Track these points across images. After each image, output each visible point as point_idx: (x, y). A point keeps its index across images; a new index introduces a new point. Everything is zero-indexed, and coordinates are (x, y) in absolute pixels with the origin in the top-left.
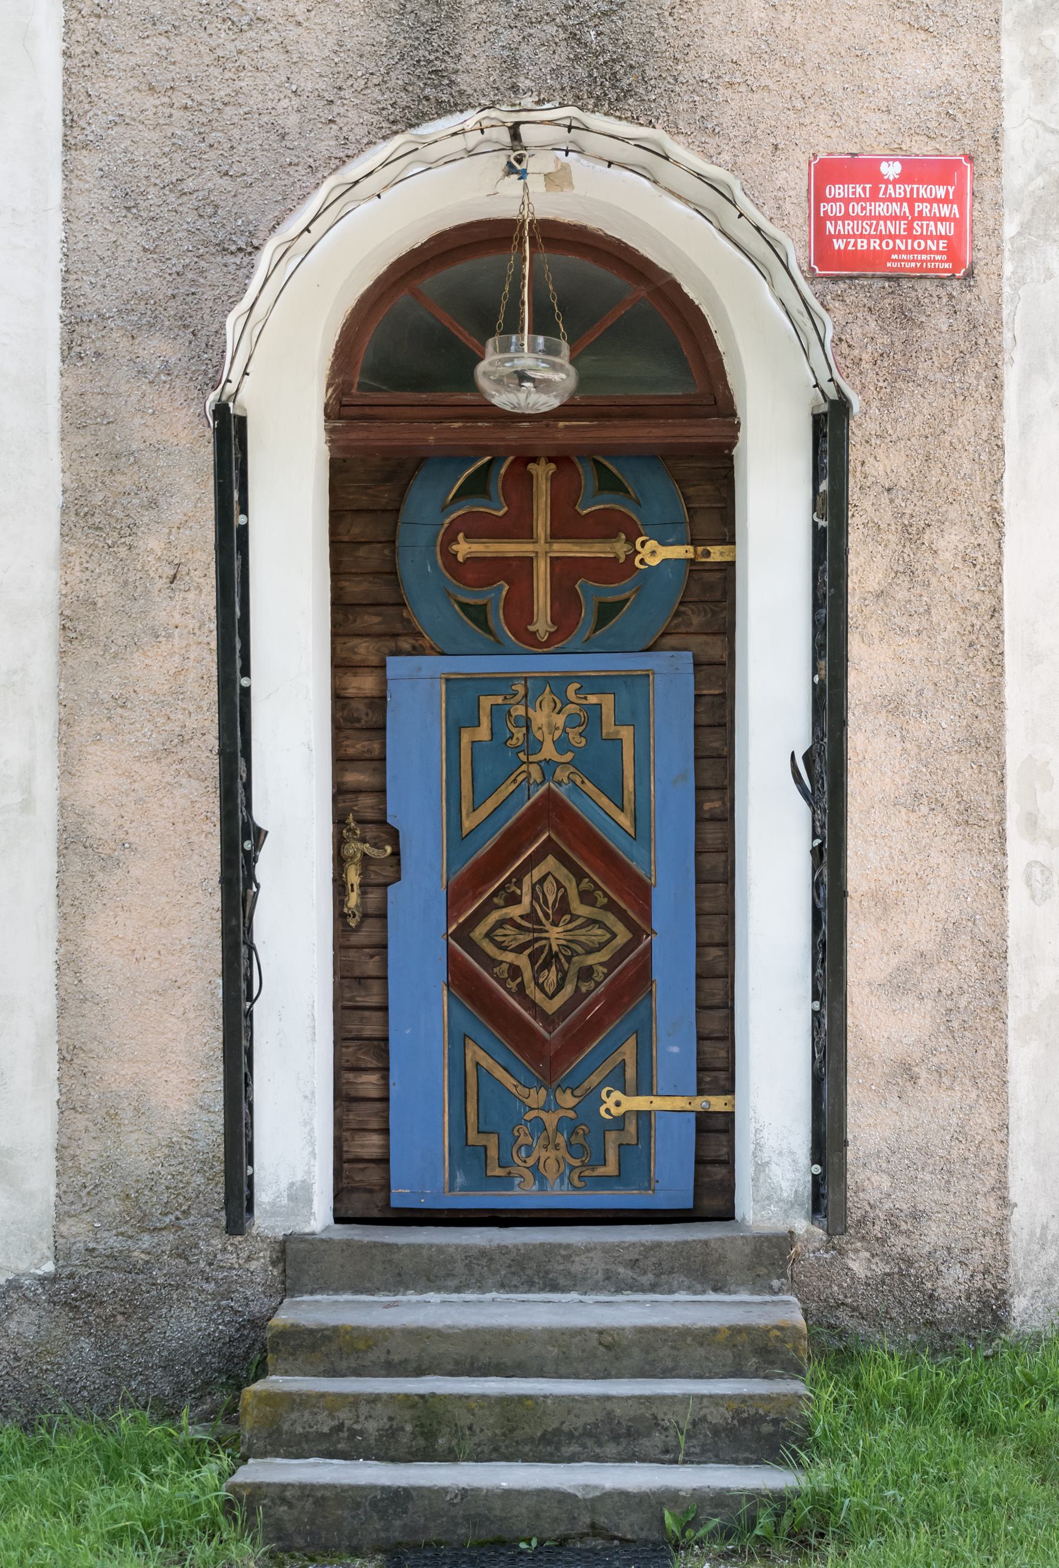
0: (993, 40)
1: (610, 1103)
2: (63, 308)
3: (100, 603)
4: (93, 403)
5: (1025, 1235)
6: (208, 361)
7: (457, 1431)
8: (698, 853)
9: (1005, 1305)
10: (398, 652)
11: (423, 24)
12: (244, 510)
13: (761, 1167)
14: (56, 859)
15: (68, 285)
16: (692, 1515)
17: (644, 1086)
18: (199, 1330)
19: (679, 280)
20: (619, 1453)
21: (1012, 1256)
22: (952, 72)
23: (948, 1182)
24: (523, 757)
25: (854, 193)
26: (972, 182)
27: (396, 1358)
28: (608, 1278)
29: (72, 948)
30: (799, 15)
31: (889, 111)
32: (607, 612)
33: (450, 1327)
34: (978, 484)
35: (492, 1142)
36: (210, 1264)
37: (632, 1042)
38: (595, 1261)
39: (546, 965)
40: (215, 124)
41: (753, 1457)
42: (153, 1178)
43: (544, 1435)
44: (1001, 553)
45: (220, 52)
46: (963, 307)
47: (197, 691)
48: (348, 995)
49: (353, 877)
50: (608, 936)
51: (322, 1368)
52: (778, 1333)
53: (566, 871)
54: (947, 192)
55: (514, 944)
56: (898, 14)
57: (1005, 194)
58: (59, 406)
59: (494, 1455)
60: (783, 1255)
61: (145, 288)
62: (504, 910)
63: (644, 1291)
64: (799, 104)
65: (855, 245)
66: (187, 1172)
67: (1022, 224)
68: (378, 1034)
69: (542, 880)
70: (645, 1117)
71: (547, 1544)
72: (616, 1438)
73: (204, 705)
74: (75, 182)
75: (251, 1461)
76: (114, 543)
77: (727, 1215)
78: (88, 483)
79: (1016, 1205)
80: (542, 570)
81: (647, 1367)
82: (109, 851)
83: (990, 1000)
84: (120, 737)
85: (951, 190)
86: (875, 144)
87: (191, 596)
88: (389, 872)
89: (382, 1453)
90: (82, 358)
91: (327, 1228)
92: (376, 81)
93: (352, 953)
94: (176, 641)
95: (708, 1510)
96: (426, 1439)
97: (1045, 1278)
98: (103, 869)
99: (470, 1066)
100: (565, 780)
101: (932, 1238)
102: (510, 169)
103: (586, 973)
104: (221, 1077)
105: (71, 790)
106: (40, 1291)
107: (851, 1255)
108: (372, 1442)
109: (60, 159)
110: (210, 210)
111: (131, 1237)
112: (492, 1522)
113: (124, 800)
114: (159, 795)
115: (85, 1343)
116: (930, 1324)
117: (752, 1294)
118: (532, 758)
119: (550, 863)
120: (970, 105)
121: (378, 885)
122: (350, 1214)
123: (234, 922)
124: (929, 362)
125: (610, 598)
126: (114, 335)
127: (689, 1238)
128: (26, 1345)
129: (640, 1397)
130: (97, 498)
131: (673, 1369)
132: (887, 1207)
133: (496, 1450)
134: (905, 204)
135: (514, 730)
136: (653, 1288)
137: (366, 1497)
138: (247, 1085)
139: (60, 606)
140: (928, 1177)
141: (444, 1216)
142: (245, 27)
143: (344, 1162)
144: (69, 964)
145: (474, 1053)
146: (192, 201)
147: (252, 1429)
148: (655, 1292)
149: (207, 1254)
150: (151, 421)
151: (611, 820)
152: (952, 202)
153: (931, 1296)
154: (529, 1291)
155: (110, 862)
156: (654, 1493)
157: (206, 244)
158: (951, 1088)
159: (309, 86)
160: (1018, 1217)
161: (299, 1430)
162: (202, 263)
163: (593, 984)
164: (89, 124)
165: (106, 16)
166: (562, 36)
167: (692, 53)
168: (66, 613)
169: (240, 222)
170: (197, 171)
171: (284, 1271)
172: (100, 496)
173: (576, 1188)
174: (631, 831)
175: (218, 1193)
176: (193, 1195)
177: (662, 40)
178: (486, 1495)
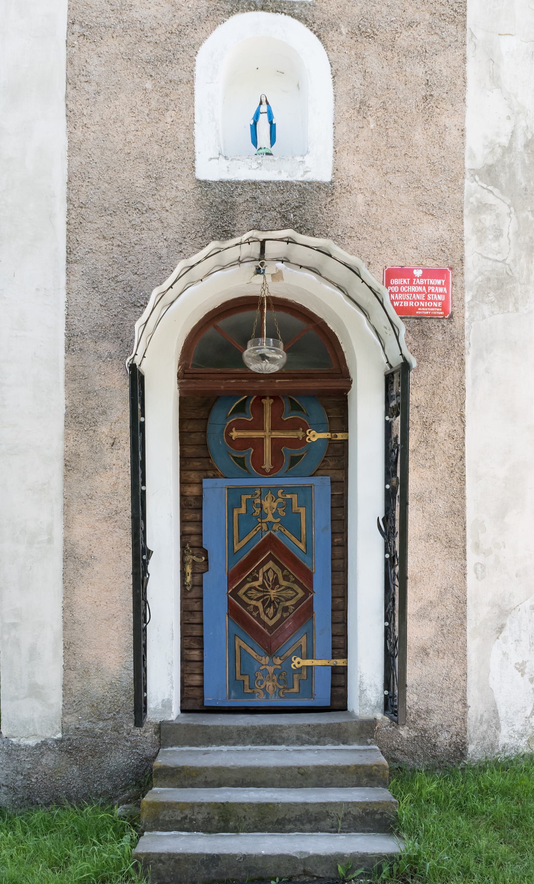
0: (460, 220)
1: (295, 663)
2: (66, 330)
3: (81, 454)
4: (79, 370)
5: (473, 719)
6: (126, 344)
7: (238, 819)
8: (332, 559)
9: (465, 748)
10: (207, 477)
11: (220, 211)
12: (143, 415)
13: (362, 692)
14: (62, 563)
15: (68, 320)
16: (350, 866)
17: (310, 655)
18: (124, 762)
19: (326, 322)
20: (311, 828)
21: (468, 728)
22: (443, 233)
23: (442, 697)
24: (259, 520)
25: (402, 282)
26: (452, 278)
27: (209, 780)
28: (298, 739)
29: (69, 601)
30: (379, 208)
31: (417, 249)
32: (294, 460)
33: (233, 766)
34: (455, 404)
35: (246, 679)
36: (128, 734)
37: (305, 637)
38: (293, 732)
39: (269, 606)
40: (131, 253)
41: (372, 829)
42: (104, 698)
43: (278, 820)
44: (464, 433)
45: (133, 223)
46: (448, 330)
47: (123, 492)
48: (186, 618)
49: (189, 570)
50: (295, 594)
51: (177, 784)
52: (376, 768)
53: (277, 567)
54: (442, 282)
55: (256, 597)
56: (421, 208)
57: (465, 283)
58: (64, 371)
59: (255, 830)
60: (372, 729)
61: (101, 322)
62: (251, 583)
63: (313, 744)
64: (379, 245)
65: (403, 304)
66: (118, 695)
67: (473, 296)
68: (198, 634)
69: (267, 571)
70: (310, 668)
71: (283, 880)
72: (310, 822)
73: (126, 497)
74: (71, 277)
75: (146, 833)
76: (88, 429)
77: (344, 708)
78: (76, 404)
79: (470, 707)
80: (268, 443)
81: (319, 783)
82: (84, 560)
83: (459, 621)
84: (90, 512)
85: (443, 281)
86: (411, 262)
87: (120, 452)
88: (203, 568)
89: (204, 829)
90: (74, 351)
91: (178, 717)
92: (200, 235)
93: (188, 601)
94: (114, 471)
95: (358, 863)
96: (224, 823)
97: (482, 737)
98: (83, 567)
99: (237, 647)
100: (277, 530)
101: (435, 721)
102: (258, 271)
103: (285, 609)
104: (132, 656)
105: (69, 534)
106: (56, 746)
107: (401, 728)
108: (200, 824)
109: (65, 267)
110: (129, 289)
111: (94, 723)
112: (258, 870)
113: (92, 538)
114: (107, 536)
115: (75, 768)
116: (433, 757)
117: (359, 745)
118: (263, 521)
119: (271, 564)
120: (451, 246)
121: (199, 573)
122: (187, 708)
123: (138, 591)
124: (434, 353)
125: (296, 455)
126: (88, 341)
127: (332, 721)
128: (49, 769)
129: (321, 803)
130: (80, 410)
131: (330, 784)
132: (416, 708)
133: (256, 827)
134: (424, 287)
135: (256, 509)
136: (317, 743)
137: (199, 859)
138: (144, 660)
139: (64, 456)
140: (433, 695)
141: (226, 709)
142: (144, 212)
143: (185, 687)
144: (68, 607)
145: (239, 642)
146: (122, 285)
147: (146, 818)
148: (318, 745)
149: (127, 730)
150: (103, 377)
151: (296, 546)
152: (444, 286)
153: (434, 745)
154: (264, 745)
155: (85, 565)
156: (332, 856)
157: (127, 303)
158: (443, 658)
159: (171, 237)
160: (471, 712)
161: (167, 819)
162: (126, 311)
163: (288, 614)
164: (78, 253)
165: (85, 208)
166: (279, 216)
167: (334, 224)
168: (67, 459)
169: (142, 294)
170: (124, 272)
171: (160, 737)
172: (82, 409)
173: (281, 697)
174: (305, 551)
175: (132, 704)
176: (121, 705)
177: (321, 218)
178: (255, 857)
